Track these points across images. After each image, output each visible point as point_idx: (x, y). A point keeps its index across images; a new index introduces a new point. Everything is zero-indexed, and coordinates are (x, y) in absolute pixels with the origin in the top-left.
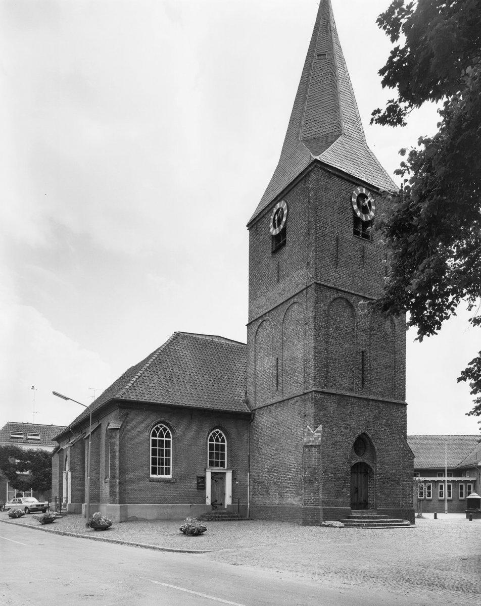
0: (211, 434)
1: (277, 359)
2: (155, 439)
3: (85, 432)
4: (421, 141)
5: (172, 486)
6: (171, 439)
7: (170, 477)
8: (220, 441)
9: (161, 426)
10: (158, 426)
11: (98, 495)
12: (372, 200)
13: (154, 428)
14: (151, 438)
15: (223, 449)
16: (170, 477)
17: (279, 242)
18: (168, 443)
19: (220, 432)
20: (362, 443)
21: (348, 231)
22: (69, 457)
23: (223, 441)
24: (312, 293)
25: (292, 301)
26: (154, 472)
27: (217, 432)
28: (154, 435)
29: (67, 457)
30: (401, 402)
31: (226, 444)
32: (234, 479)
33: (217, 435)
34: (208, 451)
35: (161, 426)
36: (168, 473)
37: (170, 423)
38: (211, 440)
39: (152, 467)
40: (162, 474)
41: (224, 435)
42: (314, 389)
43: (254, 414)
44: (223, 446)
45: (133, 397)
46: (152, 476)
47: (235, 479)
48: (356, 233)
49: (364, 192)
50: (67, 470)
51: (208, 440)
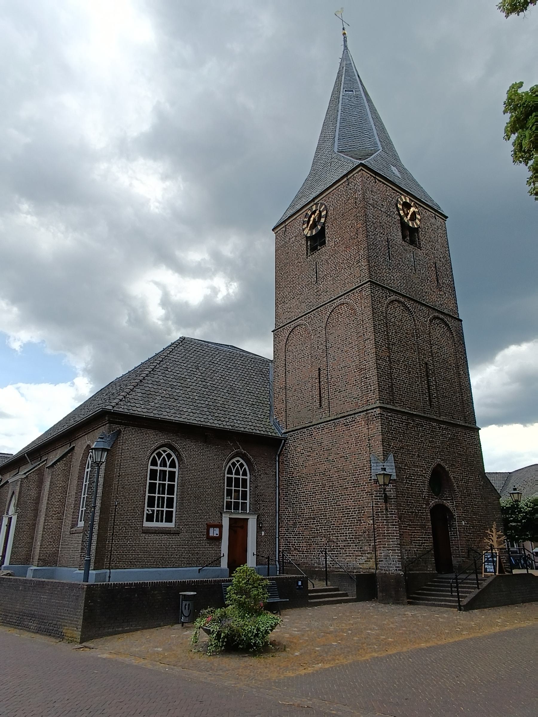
0: (230, 464)
1: (319, 369)
2: (148, 499)
3: (47, 460)
4: (505, 112)
5: (177, 538)
6: (176, 470)
7: (172, 525)
8: (241, 473)
9: (165, 451)
10: (160, 450)
11: (56, 554)
12: (416, 210)
13: (154, 454)
14: (150, 467)
15: (244, 485)
16: (172, 525)
17: (317, 241)
18: (172, 474)
19: (242, 461)
20: (439, 480)
21: (397, 235)
22: (17, 494)
23: (245, 474)
24: (366, 292)
25: (338, 301)
26: (150, 518)
27: (238, 461)
28: (154, 463)
29: (13, 493)
30: (473, 426)
31: (248, 477)
32: (259, 528)
33: (238, 465)
34: (226, 488)
35: (165, 451)
36: (169, 519)
37: (177, 446)
38: (230, 472)
39: (174, 482)
40: (162, 521)
41: (246, 466)
42: (378, 404)
43: (286, 439)
44: (244, 481)
45: (123, 409)
46: (146, 524)
47: (261, 527)
48: (404, 237)
49: (408, 201)
50: (10, 513)
51: (226, 473)
